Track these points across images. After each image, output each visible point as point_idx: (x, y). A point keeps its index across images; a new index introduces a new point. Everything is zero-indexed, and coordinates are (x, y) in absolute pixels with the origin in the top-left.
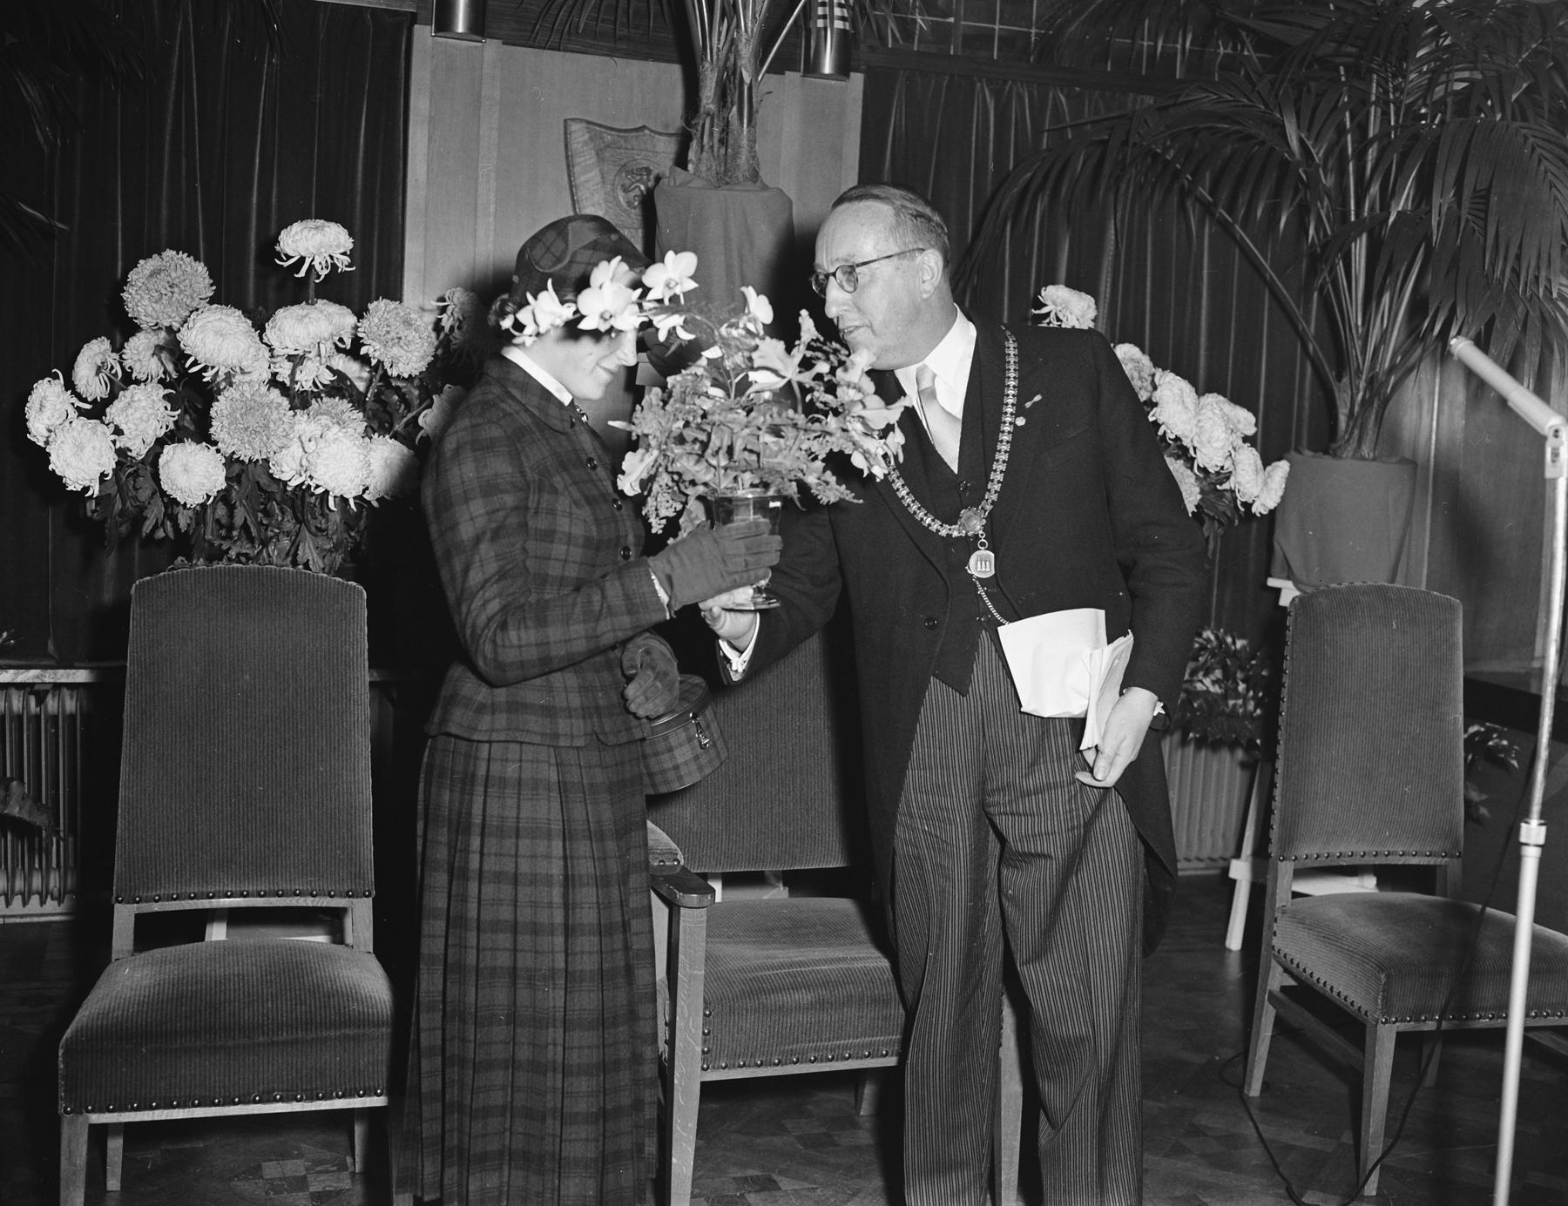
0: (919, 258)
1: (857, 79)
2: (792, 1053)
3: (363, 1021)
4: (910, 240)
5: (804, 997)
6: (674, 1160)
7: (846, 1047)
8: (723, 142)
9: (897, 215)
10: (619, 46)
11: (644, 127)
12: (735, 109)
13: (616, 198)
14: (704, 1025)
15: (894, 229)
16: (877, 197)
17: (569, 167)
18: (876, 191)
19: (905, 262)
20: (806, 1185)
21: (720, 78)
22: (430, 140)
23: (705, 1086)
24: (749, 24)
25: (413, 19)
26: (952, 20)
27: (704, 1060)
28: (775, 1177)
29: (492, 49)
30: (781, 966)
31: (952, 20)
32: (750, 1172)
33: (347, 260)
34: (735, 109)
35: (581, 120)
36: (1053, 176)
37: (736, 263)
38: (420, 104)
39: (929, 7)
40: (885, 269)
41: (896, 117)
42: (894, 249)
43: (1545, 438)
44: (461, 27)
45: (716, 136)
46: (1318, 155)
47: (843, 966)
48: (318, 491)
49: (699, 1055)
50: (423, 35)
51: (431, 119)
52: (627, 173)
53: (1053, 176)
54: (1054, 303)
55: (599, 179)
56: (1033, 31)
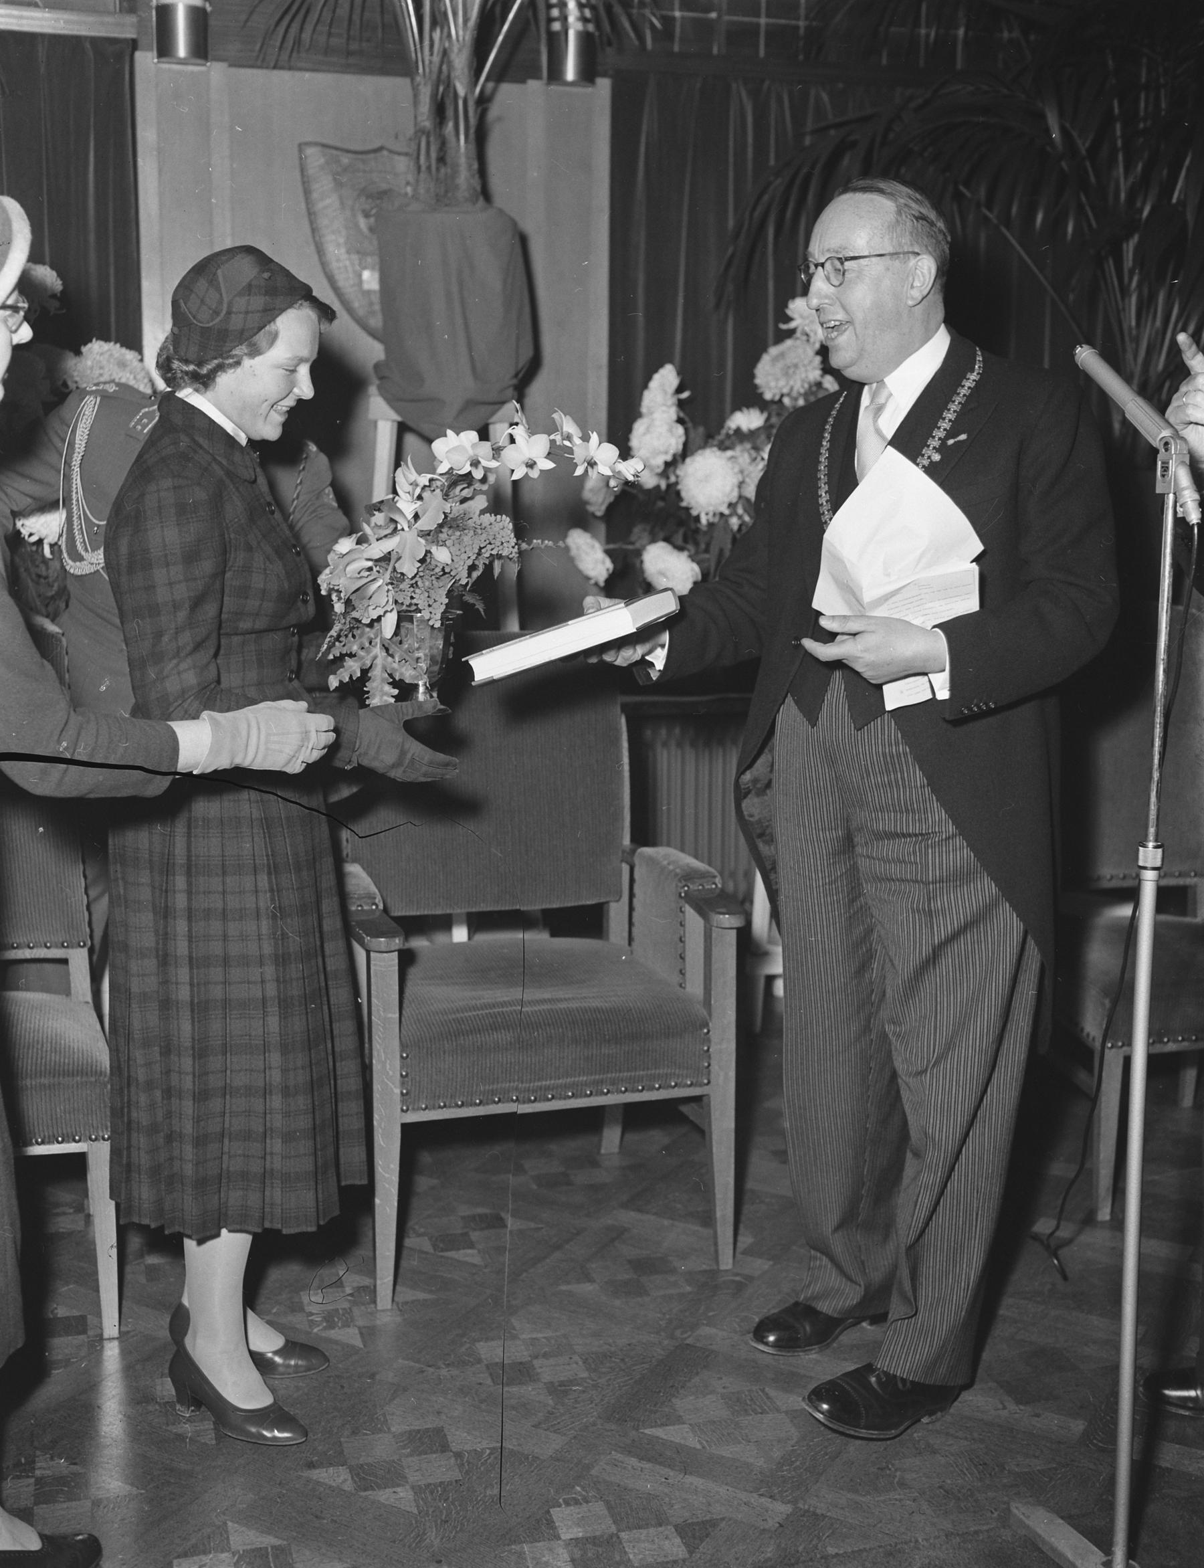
0: (913, 261)
1: (604, 85)
2: (493, 1093)
3: (83, 1071)
4: (906, 242)
5: (504, 1037)
6: (377, 1201)
7: (548, 1088)
8: (441, 160)
9: (899, 213)
10: (351, 60)
11: (381, 149)
12: (451, 125)
13: (357, 225)
14: (402, 1068)
15: (892, 227)
16: (881, 191)
17: (307, 192)
18: (882, 185)
19: (897, 263)
20: (532, 1225)
21: (434, 95)
22: (160, 171)
23: (405, 1127)
24: (460, 32)
25: (134, 45)
26: (713, 15)
27: (403, 1102)
28: (503, 1215)
29: (216, 72)
30: (485, 1007)
31: (713, 15)
32: (480, 1210)
33: (56, 304)
34: (451, 125)
35: (316, 144)
36: (798, 182)
37: (455, 289)
38: (147, 135)
39: (684, 6)
40: (874, 267)
41: (648, 124)
42: (889, 249)
43: (1156, 451)
44: (182, 50)
45: (434, 155)
46: (1083, 146)
47: (546, 1007)
48: (34, 539)
49: (398, 1098)
50: (146, 60)
51: (160, 151)
52: (368, 197)
53: (798, 182)
54: (802, 317)
55: (337, 204)
56: (802, 24)
